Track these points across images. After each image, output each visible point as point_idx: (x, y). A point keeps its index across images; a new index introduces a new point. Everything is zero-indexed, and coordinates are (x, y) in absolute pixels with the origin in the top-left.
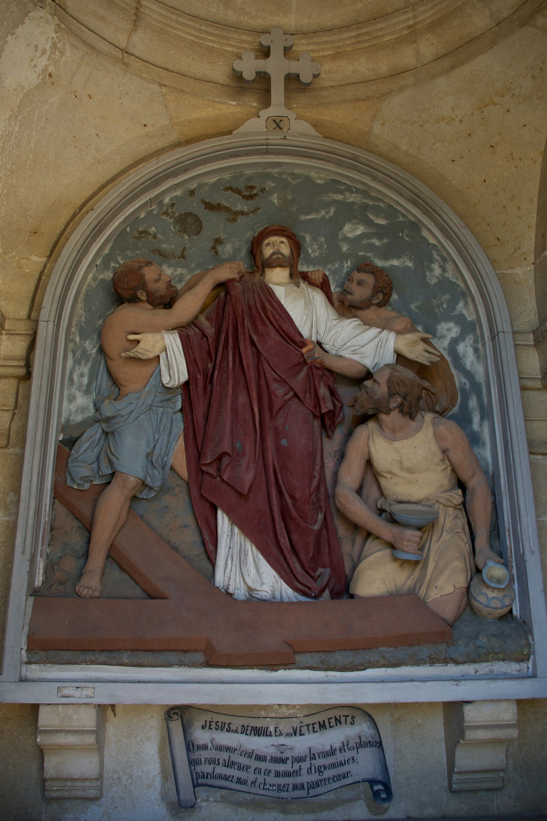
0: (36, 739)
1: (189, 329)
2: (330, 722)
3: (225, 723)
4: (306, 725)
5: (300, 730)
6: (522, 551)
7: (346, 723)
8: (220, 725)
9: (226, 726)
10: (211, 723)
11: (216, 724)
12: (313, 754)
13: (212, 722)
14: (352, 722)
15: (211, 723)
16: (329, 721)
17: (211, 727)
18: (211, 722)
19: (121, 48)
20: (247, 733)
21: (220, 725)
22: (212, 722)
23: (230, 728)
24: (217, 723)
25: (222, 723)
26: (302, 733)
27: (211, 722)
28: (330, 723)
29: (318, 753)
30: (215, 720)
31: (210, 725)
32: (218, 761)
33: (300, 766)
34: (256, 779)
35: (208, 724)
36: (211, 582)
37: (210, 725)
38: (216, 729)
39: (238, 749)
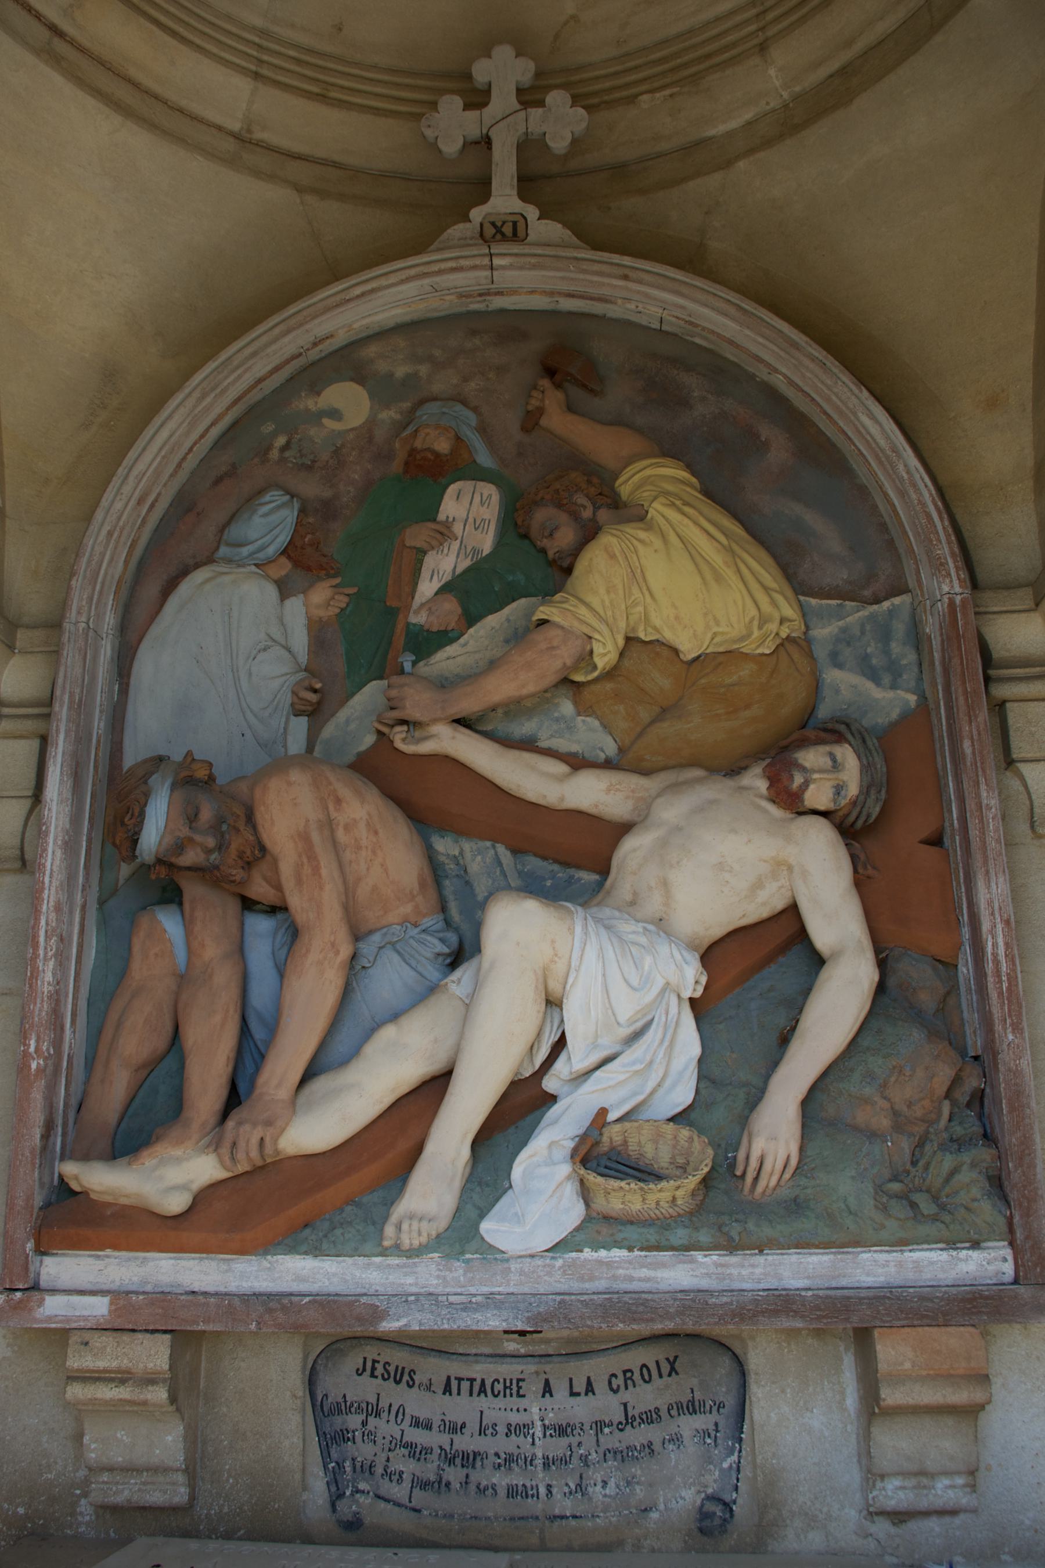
0: (65, 1392)
1: (213, 1133)
3: (403, 1368)
4: (468, 1379)
5: (519, 1388)
6: (55, 1252)
7: (459, 1394)
8: (392, 1369)
9: (406, 1377)
10: (521, 1384)
12: (457, 1451)
13: (378, 1362)
14: (411, 1383)
17: (522, 1392)
19: (822, 808)
21: (392, 1369)
23: (412, 1379)
24: (387, 1366)
25: (397, 1367)
26: (522, 1392)
27: (374, 1361)
29: (474, 1452)
30: (382, 1359)
31: (373, 1369)
32: (656, 1414)
33: (467, 1476)
35: (369, 1364)
36: (21, 1301)
37: (373, 1369)
38: (384, 1379)
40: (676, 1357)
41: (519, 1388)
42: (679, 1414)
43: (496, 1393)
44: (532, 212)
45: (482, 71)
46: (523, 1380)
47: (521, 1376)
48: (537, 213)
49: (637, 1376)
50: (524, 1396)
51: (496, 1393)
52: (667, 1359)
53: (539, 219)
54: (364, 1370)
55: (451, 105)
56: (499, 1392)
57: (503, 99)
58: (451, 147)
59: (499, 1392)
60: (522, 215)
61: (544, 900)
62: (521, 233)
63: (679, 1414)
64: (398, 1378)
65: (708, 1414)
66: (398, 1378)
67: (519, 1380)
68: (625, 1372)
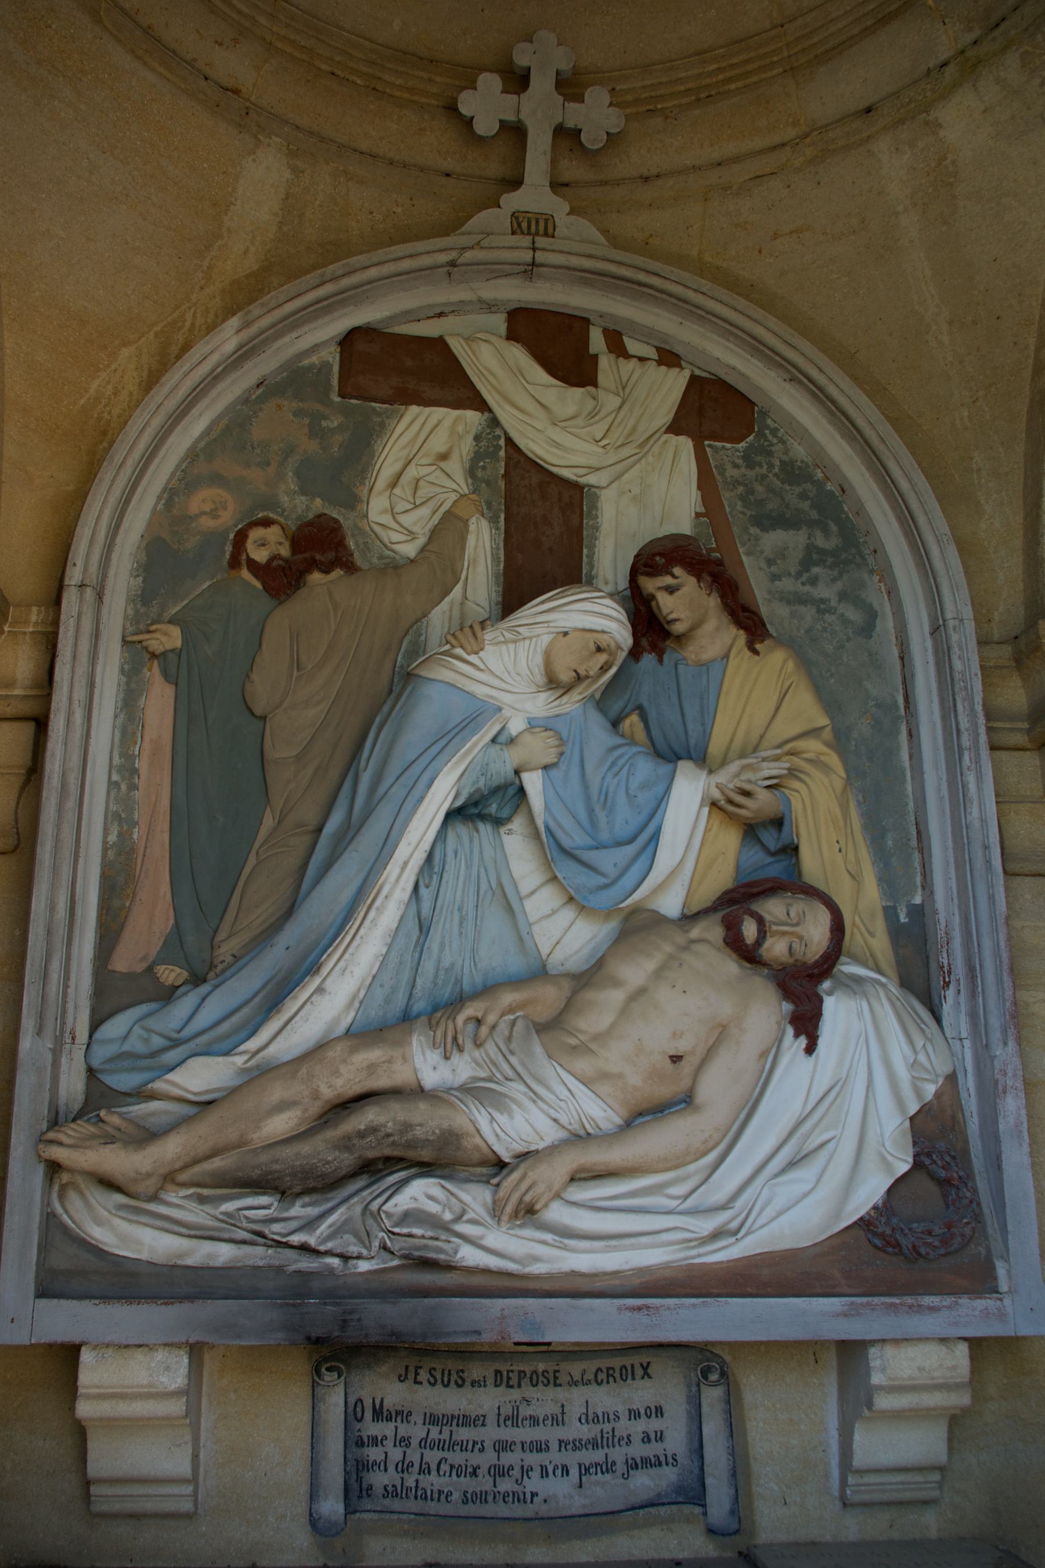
5: (556, 1378)
9: (454, 1377)
15: (511, 1374)
17: (558, 1382)
40: (649, 1363)
41: (556, 1378)
42: (552, 1425)
43: (599, 1381)
44: (557, 207)
46: (558, 1371)
48: (567, 208)
49: (617, 1375)
50: (560, 1385)
51: (599, 1381)
52: (641, 1365)
53: (568, 214)
55: (490, 82)
56: (602, 1380)
57: (542, 84)
59: (602, 1380)
60: (552, 216)
61: (225, 421)
62: (550, 231)
63: (552, 1425)
64: (624, 1370)
65: (469, 1452)
68: (608, 1369)
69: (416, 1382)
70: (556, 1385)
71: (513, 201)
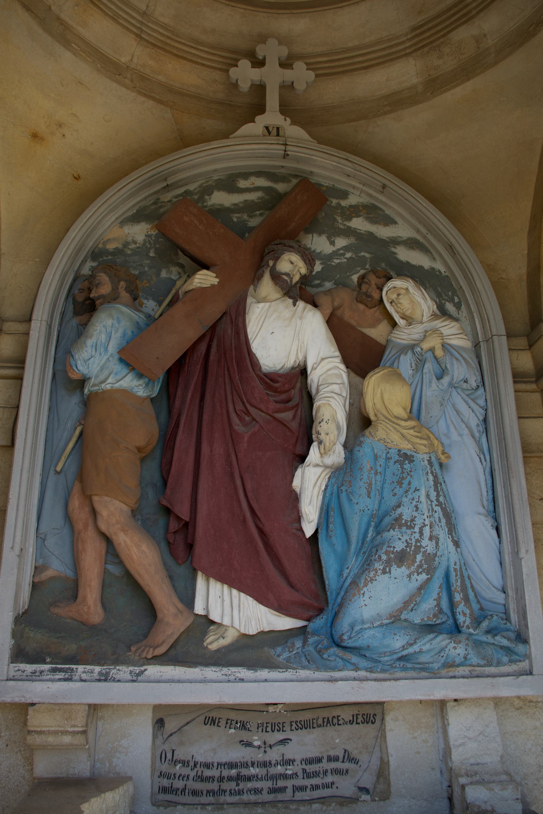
2: (220, 722)
5: (219, 722)
10: (284, 724)
11: (296, 724)
13: (359, 714)
16: (283, 725)
17: (220, 724)
18: (357, 715)
20: (358, 722)
22: (359, 714)
28: (357, 718)
34: (186, 785)
37: (357, 718)
39: (191, 759)
41: (219, 722)
45: (261, 51)
47: (358, 713)
50: (220, 726)
54: (353, 721)
55: (245, 64)
57: (272, 65)
58: (245, 86)
66: (273, 729)
67: (283, 723)
69: (357, 723)
70: (283, 731)
71: (261, 121)
